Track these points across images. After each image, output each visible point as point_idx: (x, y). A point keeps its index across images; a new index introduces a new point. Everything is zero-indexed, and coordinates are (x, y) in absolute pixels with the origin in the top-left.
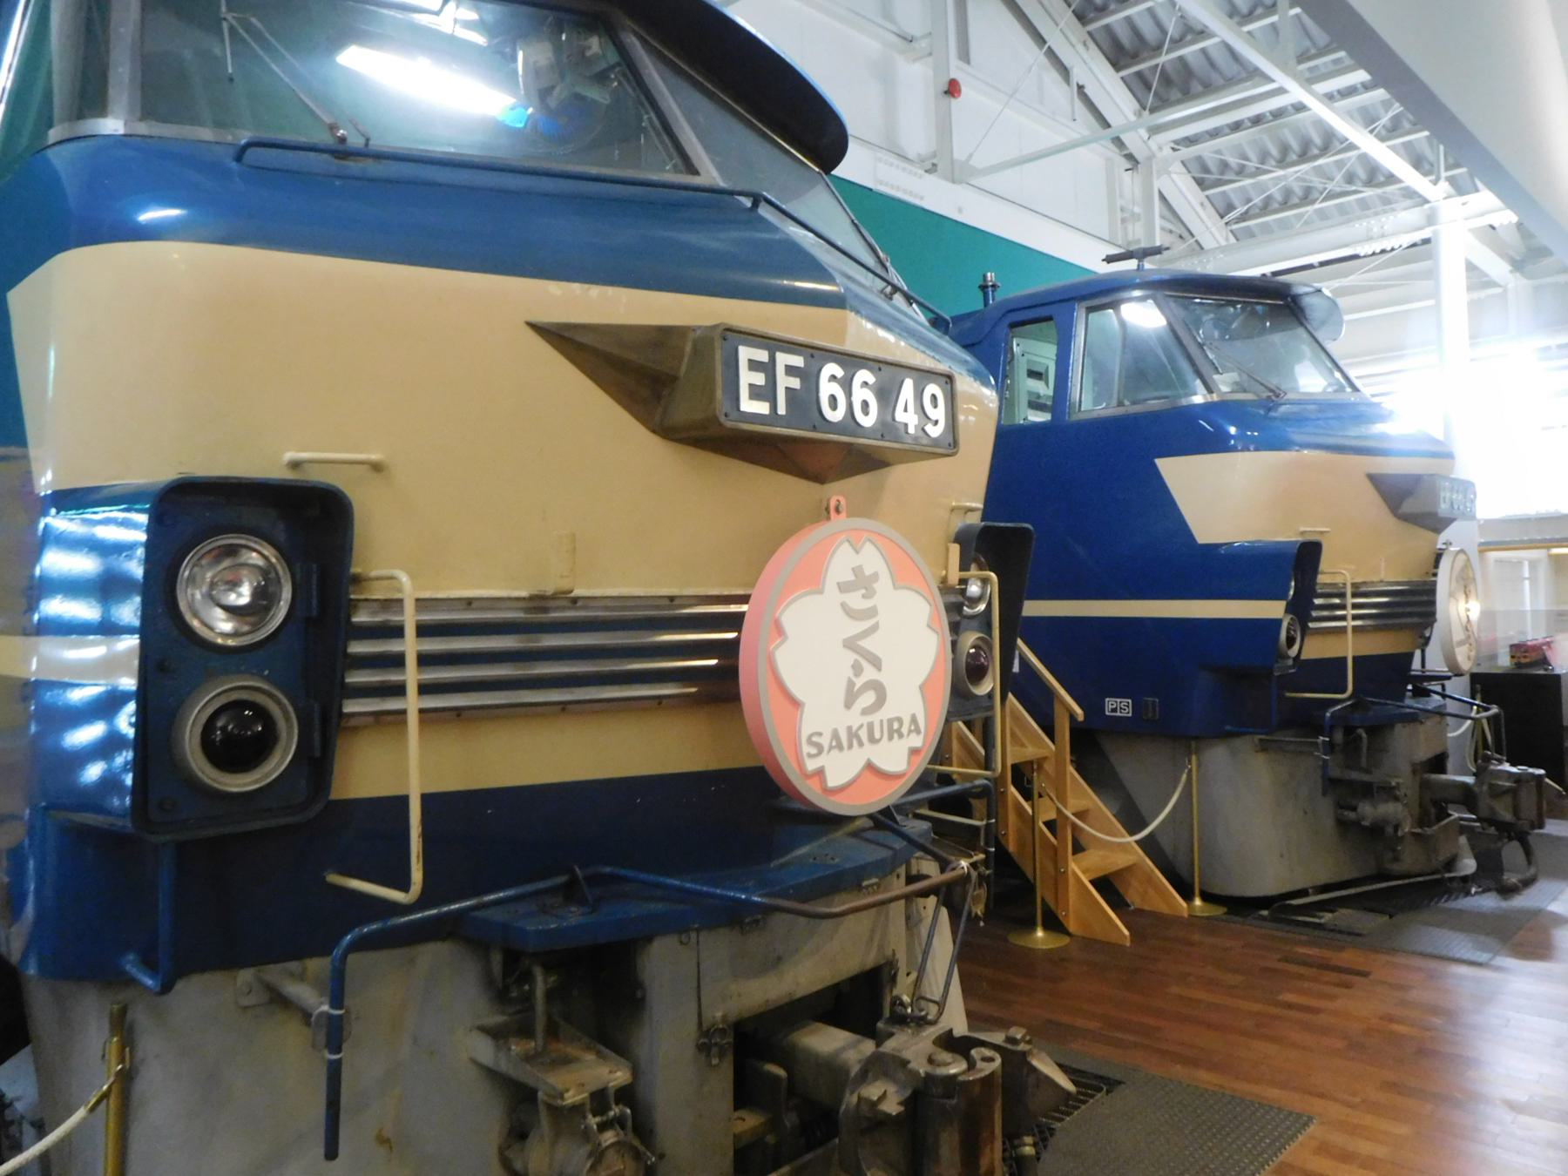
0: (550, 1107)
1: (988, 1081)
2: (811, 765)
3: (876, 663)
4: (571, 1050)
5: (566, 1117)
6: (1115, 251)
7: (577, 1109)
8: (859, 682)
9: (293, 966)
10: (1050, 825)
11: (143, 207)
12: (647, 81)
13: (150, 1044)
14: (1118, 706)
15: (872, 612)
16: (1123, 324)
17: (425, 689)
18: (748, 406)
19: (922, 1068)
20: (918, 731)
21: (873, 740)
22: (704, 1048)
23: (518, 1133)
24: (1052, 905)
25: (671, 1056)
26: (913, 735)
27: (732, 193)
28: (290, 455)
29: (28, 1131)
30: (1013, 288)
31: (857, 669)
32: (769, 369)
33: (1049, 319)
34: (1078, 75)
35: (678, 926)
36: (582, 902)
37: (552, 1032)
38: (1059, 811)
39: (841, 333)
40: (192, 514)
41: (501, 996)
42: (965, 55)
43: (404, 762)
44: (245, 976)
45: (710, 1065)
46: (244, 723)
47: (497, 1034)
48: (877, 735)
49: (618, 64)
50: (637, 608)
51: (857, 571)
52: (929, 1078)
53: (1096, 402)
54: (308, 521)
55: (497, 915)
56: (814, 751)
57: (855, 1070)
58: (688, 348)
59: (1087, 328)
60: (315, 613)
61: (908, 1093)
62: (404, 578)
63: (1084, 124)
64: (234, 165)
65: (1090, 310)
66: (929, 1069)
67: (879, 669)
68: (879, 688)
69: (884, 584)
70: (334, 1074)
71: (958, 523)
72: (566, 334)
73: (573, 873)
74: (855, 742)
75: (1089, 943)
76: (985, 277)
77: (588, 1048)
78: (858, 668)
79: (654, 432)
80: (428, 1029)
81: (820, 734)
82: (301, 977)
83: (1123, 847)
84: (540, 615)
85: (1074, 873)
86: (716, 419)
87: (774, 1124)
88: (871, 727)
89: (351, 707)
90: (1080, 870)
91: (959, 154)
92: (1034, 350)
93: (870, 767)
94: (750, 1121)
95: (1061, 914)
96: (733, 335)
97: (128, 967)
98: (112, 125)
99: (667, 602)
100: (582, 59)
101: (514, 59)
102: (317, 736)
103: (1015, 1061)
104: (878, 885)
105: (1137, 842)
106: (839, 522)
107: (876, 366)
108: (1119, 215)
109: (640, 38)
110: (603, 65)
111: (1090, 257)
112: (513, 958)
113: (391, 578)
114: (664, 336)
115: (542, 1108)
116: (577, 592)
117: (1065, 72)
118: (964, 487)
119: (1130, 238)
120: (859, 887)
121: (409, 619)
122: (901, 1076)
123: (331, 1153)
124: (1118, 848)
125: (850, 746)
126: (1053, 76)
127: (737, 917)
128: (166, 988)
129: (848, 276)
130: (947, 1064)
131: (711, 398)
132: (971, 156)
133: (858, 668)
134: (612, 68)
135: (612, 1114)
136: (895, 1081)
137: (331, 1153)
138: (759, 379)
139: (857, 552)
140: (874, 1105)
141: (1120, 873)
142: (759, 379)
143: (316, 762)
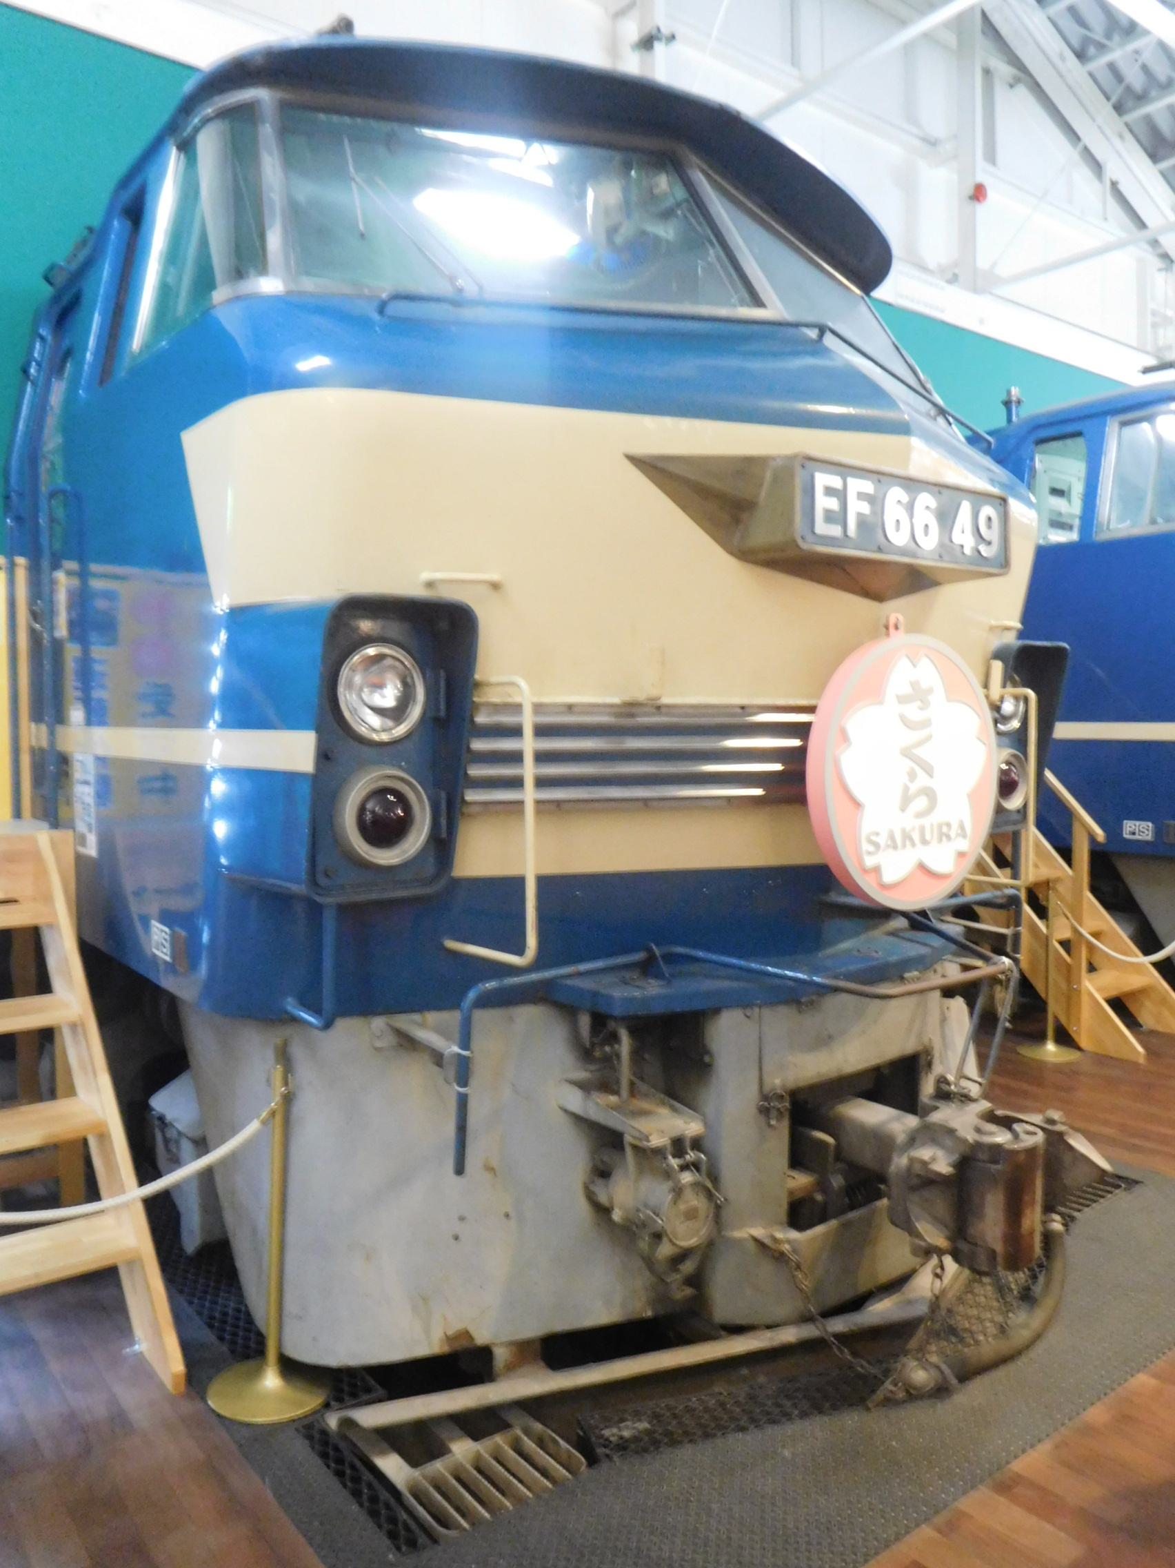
0: (635, 1147)
1: (1031, 1152)
2: (869, 862)
3: (929, 771)
4: (645, 1105)
5: (648, 1156)
6: (1152, 362)
7: (659, 1152)
8: (914, 788)
9: (416, 1017)
10: (1066, 944)
11: (305, 354)
12: (714, 216)
13: (305, 1072)
14: (1138, 830)
15: (926, 724)
16: (1159, 440)
17: (541, 782)
18: (821, 527)
19: (971, 1137)
20: (965, 836)
21: (925, 842)
22: (765, 1111)
23: (603, 1173)
24: (1063, 1020)
25: (732, 1111)
26: (960, 839)
27: (797, 325)
28: (426, 576)
29: (186, 1147)
30: (1039, 402)
31: (912, 776)
32: (841, 495)
33: (1078, 434)
34: (1113, 170)
35: (743, 1002)
36: (659, 976)
37: (633, 1092)
38: (1075, 931)
39: (905, 457)
40: (348, 622)
41: (586, 1054)
42: (991, 156)
43: (515, 846)
44: (379, 1023)
45: (770, 1126)
46: (389, 806)
47: (584, 1086)
48: (928, 837)
49: (687, 201)
50: (719, 715)
51: (915, 685)
52: (978, 1146)
53: (1121, 519)
54: (438, 634)
55: (587, 984)
56: (871, 849)
57: (901, 1138)
58: (768, 476)
59: (1115, 440)
60: (442, 714)
61: (955, 1157)
62: (523, 684)
63: (1116, 226)
64: (376, 317)
65: (1124, 424)
66: (977, 1137)
67: (931, 776)
68: (930, 794)
69: (938, 696)
70: (463, 1101)
71: (996, 642)
72: (660, 465)
73: (649, 950)
74: (908, 843)
75: (1103, 1060)
76: (1009, 392)
77: (663, 1104)
78: (916, 776)
79: (731, 553)
80: (531, 1074)
81: (877, 834)
82: (423, 1025)
83: (1137, 968)
84: (629, 720)
85: (1091, 995)
86: (795, 541)
87: (822, 1185)
88: (922, 830)
89: (471, 796)
90: (1095, 989)
91: (983, 262)
92: (1061, 466)
93: (922, 867)
94: (802, 1180)
95: (1072, 1030)
96: (811, 462)
97: (289, 1008)
98: (269, 285)
99: (739, 711)
100: (651, 197)
101: (582, 195)
102: (443, 822)
103: (1055, 1140)
104: (918, 979)
105: (1156, 965)
106: (898, 639)
107: (936, 489)
108: (1150, 319)
109: (703, 171)
110: (670, 202)
111: (1126, 371)
112: (600, 1021)
113: (512, 684)
114: (747, 467)
115: (628, 1150)
116: (666, 700)
117: (1097, 167)
118: (1000, 607)
119: (1161, 343)
120: (902, 978)
121: (528, 722)
122: (948, 1142)
123: (460, 1170)
124: (1135, 969)
125: (904, 846)
126: (1083, 173)
127: (798, 997)
128: (328, 1025)
129: (909, 405)
130: (992, 1134)
131: (791, 522)
132: (994, 264)
133: (916, 776)
134: (678, 205)
135: (688, 1157)
136: (942, 1146)
137: (460, 1170)
138: (833, 504)
139: (914, 666)
140: (925, 1164)
141: (1133, 994)
142: (833, 504)
143: (442, 845)
